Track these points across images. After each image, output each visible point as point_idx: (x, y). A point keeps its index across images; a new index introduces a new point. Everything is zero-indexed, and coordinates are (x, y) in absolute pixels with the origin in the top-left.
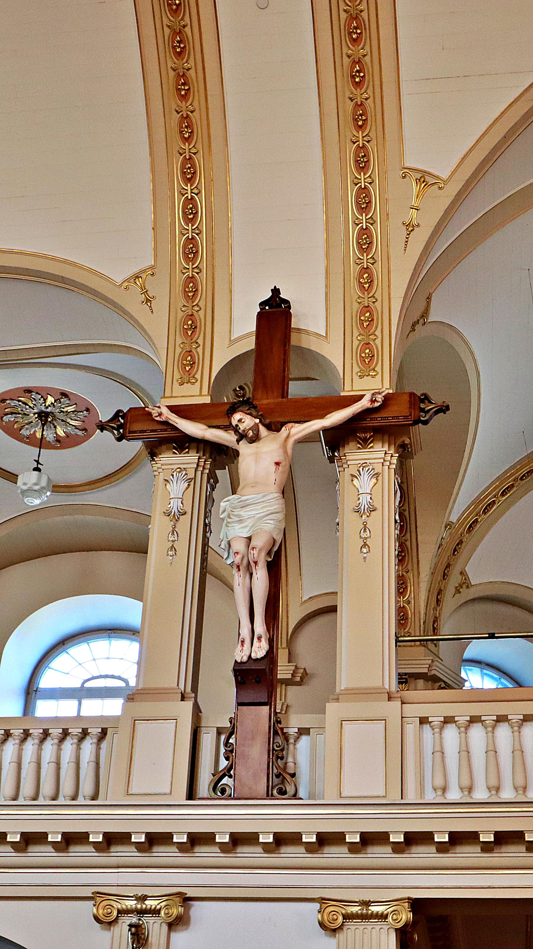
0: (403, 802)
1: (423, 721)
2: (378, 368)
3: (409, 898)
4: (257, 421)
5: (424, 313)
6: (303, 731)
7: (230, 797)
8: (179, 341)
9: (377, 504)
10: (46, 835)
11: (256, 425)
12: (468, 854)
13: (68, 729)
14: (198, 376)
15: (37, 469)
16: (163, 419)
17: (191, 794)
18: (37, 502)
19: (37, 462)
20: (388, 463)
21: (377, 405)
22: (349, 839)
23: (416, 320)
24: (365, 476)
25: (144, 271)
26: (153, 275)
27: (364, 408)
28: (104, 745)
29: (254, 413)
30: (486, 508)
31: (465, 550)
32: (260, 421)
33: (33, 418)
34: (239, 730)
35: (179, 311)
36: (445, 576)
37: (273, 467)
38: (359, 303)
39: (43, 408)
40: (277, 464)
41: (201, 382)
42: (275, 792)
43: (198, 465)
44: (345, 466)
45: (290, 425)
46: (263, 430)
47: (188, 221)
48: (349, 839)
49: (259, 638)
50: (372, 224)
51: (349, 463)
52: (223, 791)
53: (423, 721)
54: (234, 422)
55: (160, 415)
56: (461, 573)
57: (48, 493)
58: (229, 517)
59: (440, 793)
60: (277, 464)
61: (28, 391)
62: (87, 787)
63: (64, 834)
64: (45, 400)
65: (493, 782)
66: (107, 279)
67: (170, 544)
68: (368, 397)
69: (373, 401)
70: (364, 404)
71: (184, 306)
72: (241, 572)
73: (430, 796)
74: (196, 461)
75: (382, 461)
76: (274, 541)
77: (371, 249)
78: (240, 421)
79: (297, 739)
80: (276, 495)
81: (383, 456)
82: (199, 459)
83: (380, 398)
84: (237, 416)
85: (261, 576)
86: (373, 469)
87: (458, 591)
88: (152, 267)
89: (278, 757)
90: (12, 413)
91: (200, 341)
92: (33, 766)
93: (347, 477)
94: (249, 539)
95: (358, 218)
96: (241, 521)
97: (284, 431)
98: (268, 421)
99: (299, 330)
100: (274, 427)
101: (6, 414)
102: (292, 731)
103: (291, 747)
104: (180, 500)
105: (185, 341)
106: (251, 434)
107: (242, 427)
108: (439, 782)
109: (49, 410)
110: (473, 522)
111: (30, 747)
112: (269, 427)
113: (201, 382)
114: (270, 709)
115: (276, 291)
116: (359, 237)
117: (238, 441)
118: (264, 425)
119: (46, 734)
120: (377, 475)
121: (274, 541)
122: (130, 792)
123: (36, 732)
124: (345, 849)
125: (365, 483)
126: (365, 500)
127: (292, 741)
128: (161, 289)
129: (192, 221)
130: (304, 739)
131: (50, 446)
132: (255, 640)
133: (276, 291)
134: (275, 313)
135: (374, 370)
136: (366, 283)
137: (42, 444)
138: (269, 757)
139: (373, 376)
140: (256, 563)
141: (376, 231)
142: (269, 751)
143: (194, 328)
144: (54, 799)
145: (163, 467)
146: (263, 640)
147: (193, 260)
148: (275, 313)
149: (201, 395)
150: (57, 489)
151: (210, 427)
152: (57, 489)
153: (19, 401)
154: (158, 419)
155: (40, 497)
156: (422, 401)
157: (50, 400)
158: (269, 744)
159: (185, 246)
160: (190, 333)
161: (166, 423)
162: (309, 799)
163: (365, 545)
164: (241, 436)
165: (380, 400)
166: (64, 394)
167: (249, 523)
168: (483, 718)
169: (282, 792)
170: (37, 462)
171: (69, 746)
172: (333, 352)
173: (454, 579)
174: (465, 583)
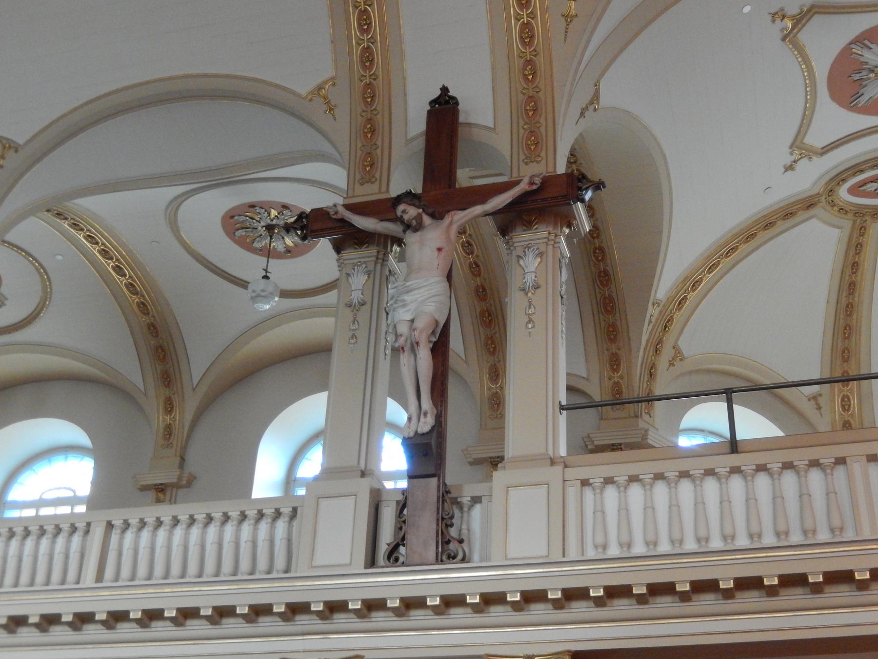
0: (564, 560)
1: (585, 483)
2: (543, 154)
3: (569, 651)
4: (421, 211)
5: (593, 98)
6: (476, 500)
7: (403, 564)
8: (359, 145)
9: (542, 282)
10: (464, 596)
11: (420, 215)
12: (621, 607)
13: (279, 509)
14: (377, 175)
15: (266, 277)
16: (339, 216)
17: (371, 562)
18: (267, 307)
19: (266, 270)
20: (552, 242)
21: (535, 187)
22: (636, 591)
23: (584, 106)
24: (530, 256)
25: (326, 82)
26: (334, 85)
27: (523, 191)
28: (295, 523)
29: (417, 203)
30: (693, 286)
31: (675, 327)
32: (424, 210)
33: (262, 231)
34: (409, 503)
35: (359, 116)
36: (657, 351)
37: (436, 253)
38: (524, 94)
39: (269, 221)
40: (439, 250)
41: (380, 180)
42: (444, 558)
43: (377, 258)
44: (512, 248)
45: (453, 212)
46: (427, 220)
47: (363, 31)
48: (636, 591)
49: (425, 414)
50: (532, 18)
51: (516, 245)
52: (397, 560)
53: (585, 483)
54: (399, 213)
55: (336, 213)
56: (674, 348)
57: (276, 299)
58: (395, 303)
59: (600, 550)
60: (439, 250)
61: (252, 206)
62: (280, 562)
63: (402, 600)
64: (269, 214)
65: (625, 538)
66: (294, 93)
67: (351, 333)
68: (526, 180)
69: (531, 183)
70: (523, 187)
71: (364, 111)
72: (406, 353)
73: (591, 554)
74: (375, 254)
75: (546, 240)
76: (437, 323)
77: (533, 43)
78: (404, 211)
79: (471, 507)
80: (437, 279)
81: (547, 235)
82: (378, 252)
83: (538, 181)
84: (401, 207)
85: (424, 356)
86: (538, 249)
87: (671, 364)
88: (333, 78)
89: (447, 526)
90: (242, 228)
91: (379, 143)
92: (267, 544)
93: (514, 259)
94: (412, 321)
95: (519, 14)
96: (404, 306)
97: (447, 220)
98: (430, 211)
99: (469, 125)
100: (437, 216)
101: (238, 230)
102: (466, 500)
103: (465, 515)
104: (360, 292)
105: (365, 143)
106: (414, 223)
107: (406, 217)
108: (600, 540)
109: (274, 222)
110: (682, 299)
111: (246, 528)
112: (433, 216)
113: (380, 180)
114: (439, 480)
115: (445, 90)
116: (522, 31)
117: (404, 231)
118: (428, 214)
119: (261, 515)
120: (541, 255)
121: (437, 323)
122: (314, 564)
123: (252, 513)
124: (807, 590)
125: (531, 263)
126: (530, 279)
127: (466, 509)
128: (342, 99)
129: (367, 31)
130: (478, 508)
131: (279, 256)
132: (422, 416)
133: (445, 90)
134: (444, 108)
135: (539, 156)
136: (529, 75)
137: (269, 253)
138: (438, 525)
139: (538, 162)
140: (417, 343)
141: (537, 25)
142: (438, 520)
143: (373, 131)
144: (251, 574)
145: (346, 262)
146: (429, 415)
147: (370, 68)
148: (444, 108)
149: (380, 192)
150: (285, 294)
151: (382, 220)
152: (285, 294)
153: (247, 216)
154: (334, 217)
155: (268, 303)
156: (580, 180)
157: (274, 213)
158: (438, 513)
159: (362, 56)
160: (369, 135)
161: (342, 221)
162: (481, 561)
163: (530, 321)
164: (407, 227)
165: (537, 182)
166: (285, 207)
167: (412, 306)
168: (616, 479)
169: (452, 557)
170: (266, 270)
171: (264, 526)
172: (502, 142)
173: (667, 352)
174: (678, 355)
